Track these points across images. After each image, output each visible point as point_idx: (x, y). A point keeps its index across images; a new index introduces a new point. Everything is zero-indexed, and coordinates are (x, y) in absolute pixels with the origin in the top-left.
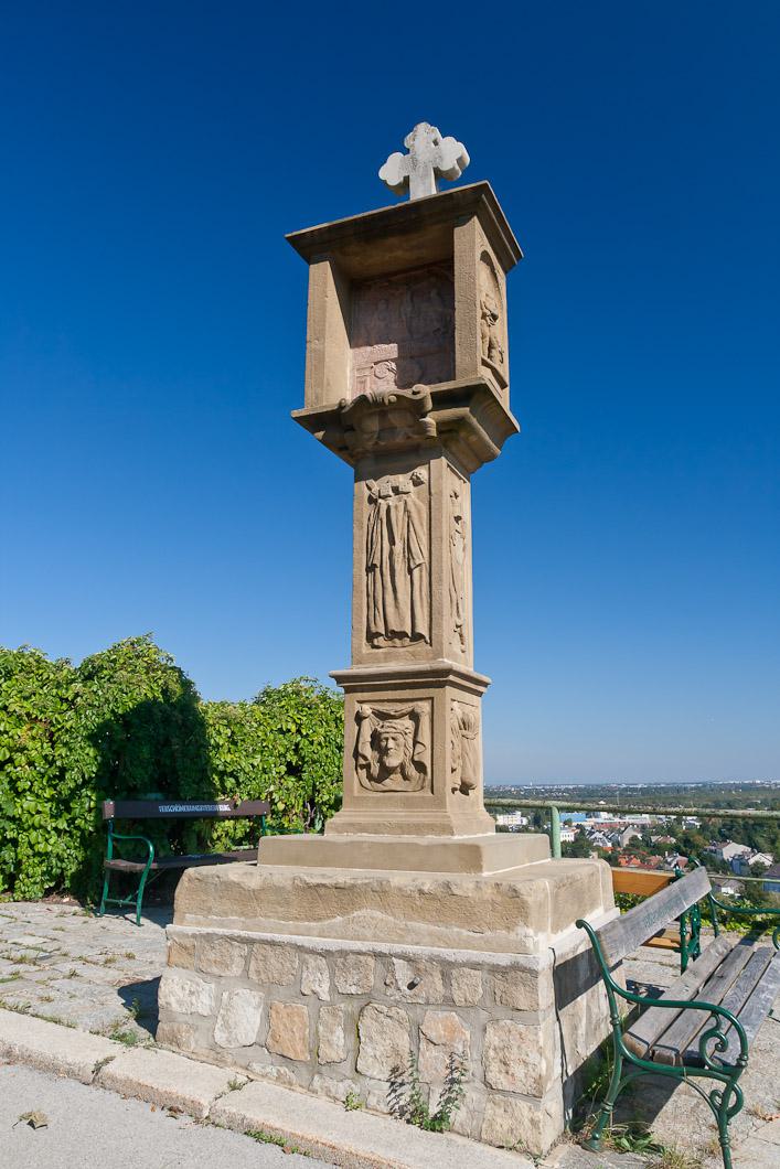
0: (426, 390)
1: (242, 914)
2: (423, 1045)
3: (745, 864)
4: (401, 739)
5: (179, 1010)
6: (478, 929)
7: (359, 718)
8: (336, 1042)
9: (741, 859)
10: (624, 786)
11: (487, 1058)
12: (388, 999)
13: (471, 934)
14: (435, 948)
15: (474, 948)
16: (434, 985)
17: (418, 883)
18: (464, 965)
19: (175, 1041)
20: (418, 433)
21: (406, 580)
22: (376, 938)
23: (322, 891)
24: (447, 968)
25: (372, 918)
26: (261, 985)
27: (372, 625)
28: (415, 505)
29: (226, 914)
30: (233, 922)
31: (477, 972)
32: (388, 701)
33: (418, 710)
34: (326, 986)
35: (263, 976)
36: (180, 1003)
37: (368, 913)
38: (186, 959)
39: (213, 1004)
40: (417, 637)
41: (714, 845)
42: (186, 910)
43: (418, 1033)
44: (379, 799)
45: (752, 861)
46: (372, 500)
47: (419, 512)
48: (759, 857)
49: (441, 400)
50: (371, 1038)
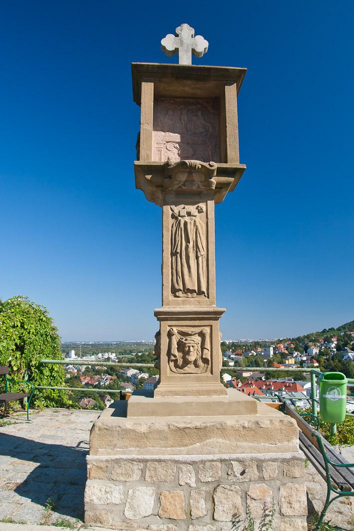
0: (216, 165)
1: (138, 446)
2: (249, 501)
3: (136, 378)
4: (196, 347)
5: (99, 503)
6: (274, 443)
7: (170, 335)
8: (201, 507)
9: (135, 376)
10: (83, 343)
11: (281, 502)
12: (229, 482)
13: (271, 445)
14: (253, 454)
15: (272, 452)
16: (253, 472)
17: (241, 422)
18: (269, 460)
19: (98, 520)
20: (205, 186)
21: (194, 262)
22: (220, 452)
23: (187, 431)
24: (260, 464)
25: (217, 442)
26: (153, 483)
27: (176, 285)
28: (200, 223)
29: (127, 447)
30: (132, 451)
31: (275, 463)
32: (187, 326)
33: (204, 331)
34: (193, 479)
35: (154, 479)
36: (100, 499)
37: (216, 440)
38: (101, 474)
39: (123, 497)
40: (200, 293)
41: (124, 370)
42: (98, 447)
43: (246, 496)
44: (181, 377)
45: (139, 377)
46: (173, 216)
47: (202, 227)
48: (143, 375)
49: (222, 172)
50: (221, 502)
